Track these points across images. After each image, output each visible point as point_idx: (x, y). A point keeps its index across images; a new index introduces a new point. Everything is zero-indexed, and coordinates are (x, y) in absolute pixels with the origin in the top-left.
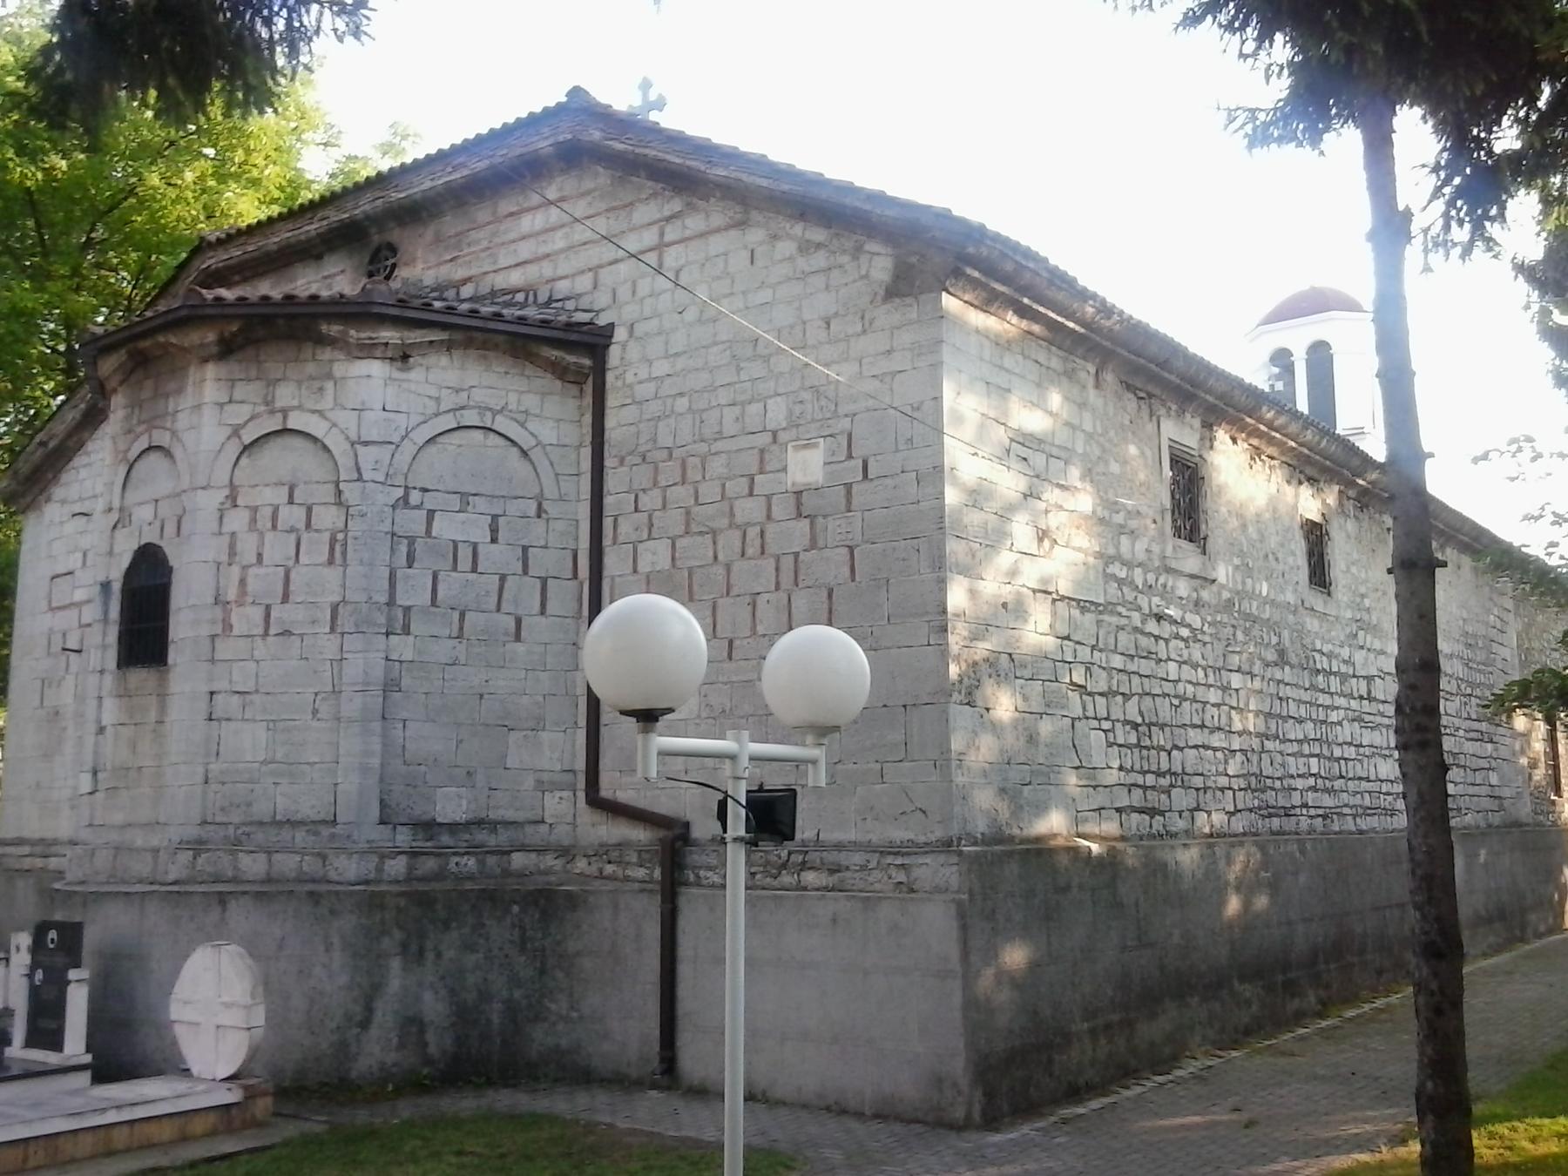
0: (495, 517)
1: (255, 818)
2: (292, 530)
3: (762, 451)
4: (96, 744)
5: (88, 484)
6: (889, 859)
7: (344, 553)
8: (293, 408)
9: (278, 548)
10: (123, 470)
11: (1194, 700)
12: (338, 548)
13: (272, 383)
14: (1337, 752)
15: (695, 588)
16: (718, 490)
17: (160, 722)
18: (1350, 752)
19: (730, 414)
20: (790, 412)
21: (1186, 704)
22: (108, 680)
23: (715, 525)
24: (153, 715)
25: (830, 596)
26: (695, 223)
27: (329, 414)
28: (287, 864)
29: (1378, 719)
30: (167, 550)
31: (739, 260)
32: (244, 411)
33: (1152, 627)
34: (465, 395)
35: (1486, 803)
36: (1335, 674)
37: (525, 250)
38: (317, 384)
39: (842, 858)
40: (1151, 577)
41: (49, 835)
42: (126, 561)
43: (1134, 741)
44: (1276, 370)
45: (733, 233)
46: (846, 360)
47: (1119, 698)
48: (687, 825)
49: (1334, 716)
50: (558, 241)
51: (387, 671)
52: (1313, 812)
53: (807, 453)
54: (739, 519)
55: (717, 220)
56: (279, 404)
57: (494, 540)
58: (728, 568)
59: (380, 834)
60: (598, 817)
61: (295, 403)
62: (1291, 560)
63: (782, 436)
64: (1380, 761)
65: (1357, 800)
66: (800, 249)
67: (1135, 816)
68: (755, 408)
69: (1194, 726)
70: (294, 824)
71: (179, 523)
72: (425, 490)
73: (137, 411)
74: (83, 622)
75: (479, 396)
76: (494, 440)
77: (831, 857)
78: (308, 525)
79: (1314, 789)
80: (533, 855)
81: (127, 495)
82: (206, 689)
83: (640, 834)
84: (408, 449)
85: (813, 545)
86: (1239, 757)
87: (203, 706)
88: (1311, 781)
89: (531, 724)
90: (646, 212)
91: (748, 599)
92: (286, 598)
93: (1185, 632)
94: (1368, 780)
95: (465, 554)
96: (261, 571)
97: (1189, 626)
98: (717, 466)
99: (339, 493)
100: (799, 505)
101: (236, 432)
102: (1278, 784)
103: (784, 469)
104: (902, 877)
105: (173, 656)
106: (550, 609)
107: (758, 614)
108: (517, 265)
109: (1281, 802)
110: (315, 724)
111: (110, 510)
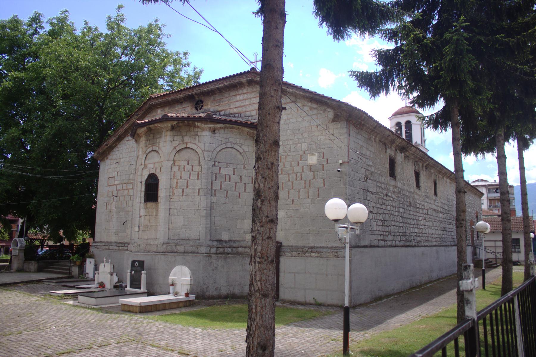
0: (234, 169)
1: (181, 238)
2: (189, 171)
4: (139, 220)
5: (118, 155)
6: (333, 250)
9: (185, 175)
10: (145, 156)
11: (393, 215)
12: (199, 176)
13: (183, 137)
14: (421, 227)
15: (284, 187)
16: (290, 164)
17: (157, 215)
18: (423, 227)
19: (292, 147)
20: (308, 147)
21: (392, 216)
22: (142, 205)
23: (289, 172)
24: (155, 213)
25: (318, 190)
27: (197, 144)
29: (429, 219)
30: (158, 175)
32: (177, 143)
33: (385, 198)
34: (227, 140)
35: (451, 240)
36: (421, 208)
37: (238, 104)
38: (194, 137)
39: (321, 250)
40: (385, 186)
41: (109, 241)
42: (146, 177)
43: (381, 224)
44: (397, 128)
46: (323, 135)
47: (379, 214)
48: (281, 243)
49: (420, 218)
50: (247, 103)
51: (211, 204)
52: (415, 241)
53: (313, 157)
54: (295, 171)
56: (185, 141)
57: (234, 174)
58: (292, 183)
59: (210, 243)
61: (189, 141)
62: (412, 181)
63: (306, 152)
64: (429, 229)
65: (424, 239)
66: (310, 109)
67: (381, 241)
68: (299, 145)
69: (393, 221)
70: (189, 240)
71: (161, 169)
72: (219, 162)
73: (148, 141)
74: (118, 189)
75: (231, 140)
76: (234, 150)
77: (318, 250)
78: (192, 170)
79: (416, 236)
80: (243, 249)
81: (146, 161)
84: (215, 152)
85: (314, 178)
86: (401, 228)
87: (168, 212)
88: (415, 234)
89: (242, 218)
91: (297, 190)
92: (187, 187)
93: (392, 199)
94: (427, 234)
95: (228, 177)
97: (392, 197)
98: (289, 158)
99: (200, 162)
100: (310, 169)
101: (175, 148)
102: (409, 234)
103: (307, 160)
104: (336, 254)
105: (159, 200)
106: (247, 191)
107: (300, 194)
108: (236, 108)
109: (409, 239)
111: (142, 165)
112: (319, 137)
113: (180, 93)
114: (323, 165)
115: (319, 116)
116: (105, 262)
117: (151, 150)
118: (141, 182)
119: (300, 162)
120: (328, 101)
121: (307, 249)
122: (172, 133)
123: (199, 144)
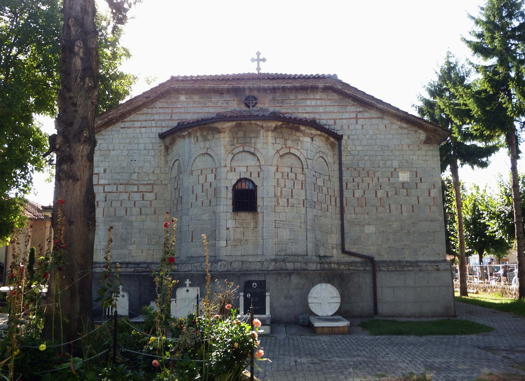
1: (288, 254)
2: (292, 179)
3: (392, 173)
7: (306, 187)
8: (292, 147)
9: (289, 184)
13: (286, 140)
19: (381, 163)
22: (229, 215)
26: (367, 115)
27: (300, 150)
28: (298, 265)
31: (382, 127)
32: (280, 146)
37: (308, 110)
45: (379, 120)
46: (415, 155)
48: (373, 258)
50: (321, 110)
55: (374, 115)
60: (344, 255)
61: (292, 146)
63: (397, 170)
68: (389, 162)
82: (274, 219)
83: (358, 259)
90: (350, 109)
96: (286, 189)
100: (403, 186)
101: (278, 151)
103: (398, 177)
108: (306, 113)
110: (300, 230)
112: (411, 157)
113: (224, 82)
114: (417, 184)
115: (410, 136)
116: (188, 285)
117: (242, 150)
118: (227, 188)
119: (391, 179)
120: (424, 123)
121: (405, 263)
122: (273, 134)
123: (302, 151)
